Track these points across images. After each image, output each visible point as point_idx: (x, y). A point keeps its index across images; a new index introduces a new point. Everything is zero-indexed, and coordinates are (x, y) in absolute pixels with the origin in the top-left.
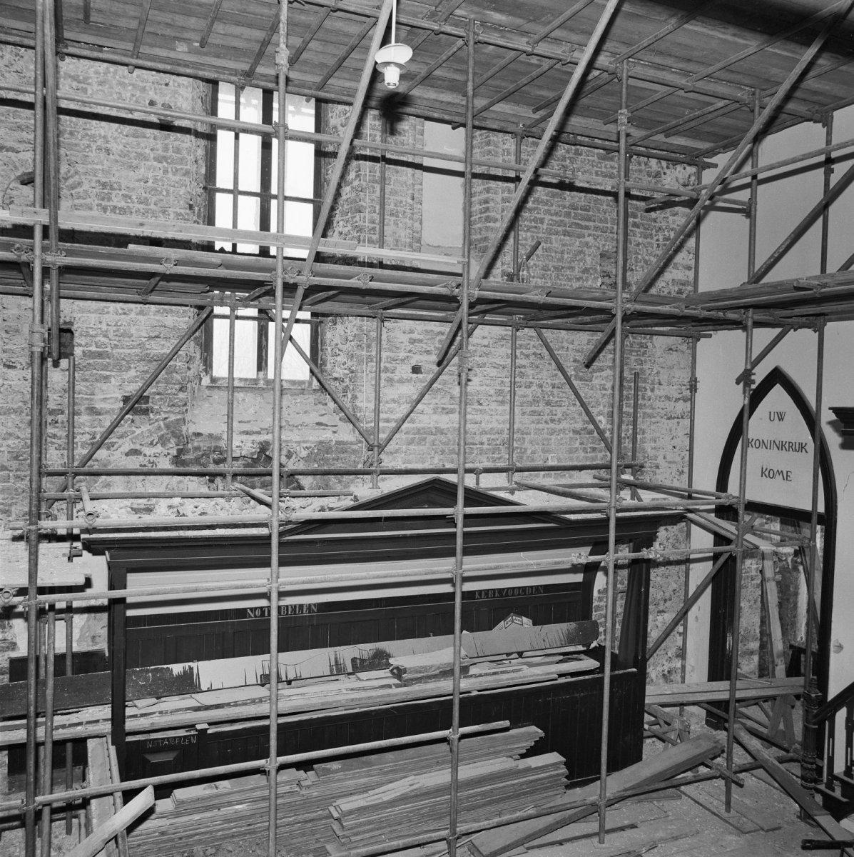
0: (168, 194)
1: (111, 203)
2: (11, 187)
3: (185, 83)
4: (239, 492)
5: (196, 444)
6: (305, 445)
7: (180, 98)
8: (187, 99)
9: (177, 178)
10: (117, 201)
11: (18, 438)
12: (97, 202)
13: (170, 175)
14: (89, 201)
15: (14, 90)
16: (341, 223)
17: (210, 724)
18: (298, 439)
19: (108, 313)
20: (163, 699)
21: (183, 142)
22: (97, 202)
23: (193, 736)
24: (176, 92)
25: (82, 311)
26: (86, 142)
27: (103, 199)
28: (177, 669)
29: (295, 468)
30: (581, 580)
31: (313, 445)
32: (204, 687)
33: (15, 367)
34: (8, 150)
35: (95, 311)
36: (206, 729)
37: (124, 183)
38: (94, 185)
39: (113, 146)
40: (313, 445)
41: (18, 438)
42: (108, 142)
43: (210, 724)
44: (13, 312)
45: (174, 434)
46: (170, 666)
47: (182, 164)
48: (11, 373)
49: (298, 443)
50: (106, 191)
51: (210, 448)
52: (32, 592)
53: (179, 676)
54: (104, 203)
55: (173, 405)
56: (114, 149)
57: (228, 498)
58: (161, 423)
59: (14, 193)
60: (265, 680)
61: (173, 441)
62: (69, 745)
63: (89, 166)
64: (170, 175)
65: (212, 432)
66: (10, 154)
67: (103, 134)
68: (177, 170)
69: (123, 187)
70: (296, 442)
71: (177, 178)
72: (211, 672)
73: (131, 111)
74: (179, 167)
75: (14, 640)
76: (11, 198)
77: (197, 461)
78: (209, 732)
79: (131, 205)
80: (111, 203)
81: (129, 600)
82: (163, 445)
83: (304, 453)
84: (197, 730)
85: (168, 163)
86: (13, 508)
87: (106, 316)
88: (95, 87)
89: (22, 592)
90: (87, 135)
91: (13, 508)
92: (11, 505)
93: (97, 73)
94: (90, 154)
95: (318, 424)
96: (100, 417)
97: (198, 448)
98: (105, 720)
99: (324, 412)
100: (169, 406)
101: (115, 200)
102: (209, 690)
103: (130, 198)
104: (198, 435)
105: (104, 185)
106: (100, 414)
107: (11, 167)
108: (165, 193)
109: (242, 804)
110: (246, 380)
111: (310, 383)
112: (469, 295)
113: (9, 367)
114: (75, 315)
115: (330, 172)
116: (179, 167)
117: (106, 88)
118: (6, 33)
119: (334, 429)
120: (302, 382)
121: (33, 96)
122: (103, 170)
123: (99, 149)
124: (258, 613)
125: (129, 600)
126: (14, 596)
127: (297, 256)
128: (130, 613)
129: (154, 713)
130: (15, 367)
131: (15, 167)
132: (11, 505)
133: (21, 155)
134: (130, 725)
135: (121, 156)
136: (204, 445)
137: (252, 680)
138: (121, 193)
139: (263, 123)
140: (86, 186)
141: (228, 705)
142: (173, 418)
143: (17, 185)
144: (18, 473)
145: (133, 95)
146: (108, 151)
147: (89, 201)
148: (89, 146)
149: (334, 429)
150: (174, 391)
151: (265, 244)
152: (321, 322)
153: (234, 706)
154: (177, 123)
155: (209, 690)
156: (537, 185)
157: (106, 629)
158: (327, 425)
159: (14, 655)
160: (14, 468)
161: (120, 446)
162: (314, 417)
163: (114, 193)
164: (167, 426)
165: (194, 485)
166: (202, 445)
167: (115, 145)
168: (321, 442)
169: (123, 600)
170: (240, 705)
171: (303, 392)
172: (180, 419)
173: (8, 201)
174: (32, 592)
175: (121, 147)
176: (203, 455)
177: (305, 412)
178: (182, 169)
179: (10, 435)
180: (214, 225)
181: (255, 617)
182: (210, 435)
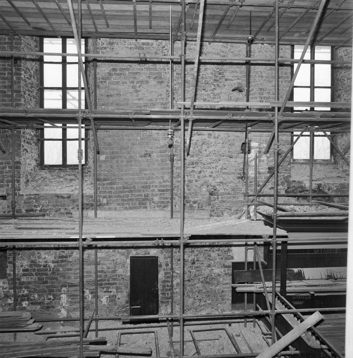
0: (283, 91)
1: (263, 96)
2: (231, 93)
3: (288, 47)
4: (315, 203)
5: (293, 185)
6: (335, 185)
7: (287, 54)
8: (289, 53)
9: (286, 84)
10: (266, 95)
11: (234, 183)
12: (259, 96)
13: (283, 83)
14: (256, 96)
15: (262, 60)
16: (345, 95)
17: (315, 292)
18: (332, 183)
19: (263, 136)
20: (291, 281)
21: (288, 70)
22: (259, 96)
23: (309, 296)
24: (285, 51)
25: (254, 136)
26: (254, 74)
27: (261, 94)
28: (296, 270)
29: (331, 194)
30: (280, 249)
31: (338, 185)
32: (306, 278)
33: (233, 157)
34: (229, 80)
35: (259, 136)
36: (314, 294)
37: (268, 88)
38: (257, 89)
39: (264, 74)
40: (338, 185)
41: (234, 183)
42: (262, 73)
43: (315, 292)
44: (232, 138)
45: (286, 181)
46: (293, 269)
47: (287, 78)
48: (232, 160)
49: (333, 184)
50: (261, 91)
51: (298, 186)
52: (274, 237)
53: (297, 273)
54: (261, 96)
55: (286, 170)
56: (264, 76)
57: (311, 206)
58: (282, 177)
59: (232, 95)
60: (329, 277)
61: (286, 184)
62: (246, 294)
63: (256, 83)
64: (283, 83)
65: (299, 180)
66: (230, 81)
67: (260, 70)
68: (286, 81)
69: (267, 89)
70: (331, 184)
71: (286, 84)
72: (308, 272)
73: (269, 61)
74: (286, 80)
75: (233, 256)
76: (231, 97)
77: (293, 191)
78: (315, 295)
79: (270, 96)
80: (263, 96)
81: (288, 242)
82: (283, 185)
83: (335, 189)
84: (310, 294)
85: (282, 79)
86: (232, 208)
87: (263, 138)
88: (257, 54)
89: (271, 237)
90: (255, 71)
91: (232, 208)
92: (231, 207)
93: (258, 48)
94: (256, 78)
95: (338, 177)
96: (261, 175)
97: (294, 187)
98: (271, 287)
99: (338, 172)
100: (285, 170)
101: (265, 94)
102: (308, 279)
103: (270, 93)
104: (295, 181)
105: (261, 89)
106: (261, 174)
107: (231, 86)
108: (282, 90)
109: (329, 324)
110: (306, 160)
111: (330, 160)
112: (278, 120)
113: (231, 157)
114: (252, 138)
115: (338, 75)
116: (286, 80)
117: (261, 54)
118: (235, 39)
119: (345, 179)
120: (328, 160)
121: (77, 57)
122: (260, 84)
123: (259, 76)
124: (318, 251)
125: (288, 242)
126: (269, 238)
127: (321, 110)
128: (289, 247)
129: (293, 286)
130: (233, 157)
131: (232, 86)
132: (231, 207)
133: (233, 82)
134: (288, 289)
135: (266, 78)
136: (296, 185)
137: (324, 277)
138: (267, 91)
139: (63, 52)
140: (255, 90)
141: (319, 285)
142: (286, 175)
143: (232, 92)
144: (234, 196)
145: (270, 55)
146: (262, 77)
147: (256, 96)
148: (255, 76)
149: (345, 179)
150: (286, 165)
151: (313, 106)
152: (335, 136)
153: (321, 286)
154: (286, 63)
155: (308, 279)
156: (201, 64)
157: (263, 254)
158: (341, 177)
159: (233, 261)
160: (233, 194)
161: (268, 186)
162: (335, 174)
163: (264, 92)
164: (284, 178)
165: (293, 200)
166: (295, 185)
167: (264, 74)
168: (341, 184)
169: (286, 242)
170: (324, 286)
171: (328, 164)
172: (289, 175)
173: (229, 98)
174: (274, 237)
175: (266, 74)
176: (295, 189)
177: (331, 172)
178: (288, 80)
179: (231, 182)
180: (293, 100)
181: (317, 252)
182: (299, 182)
